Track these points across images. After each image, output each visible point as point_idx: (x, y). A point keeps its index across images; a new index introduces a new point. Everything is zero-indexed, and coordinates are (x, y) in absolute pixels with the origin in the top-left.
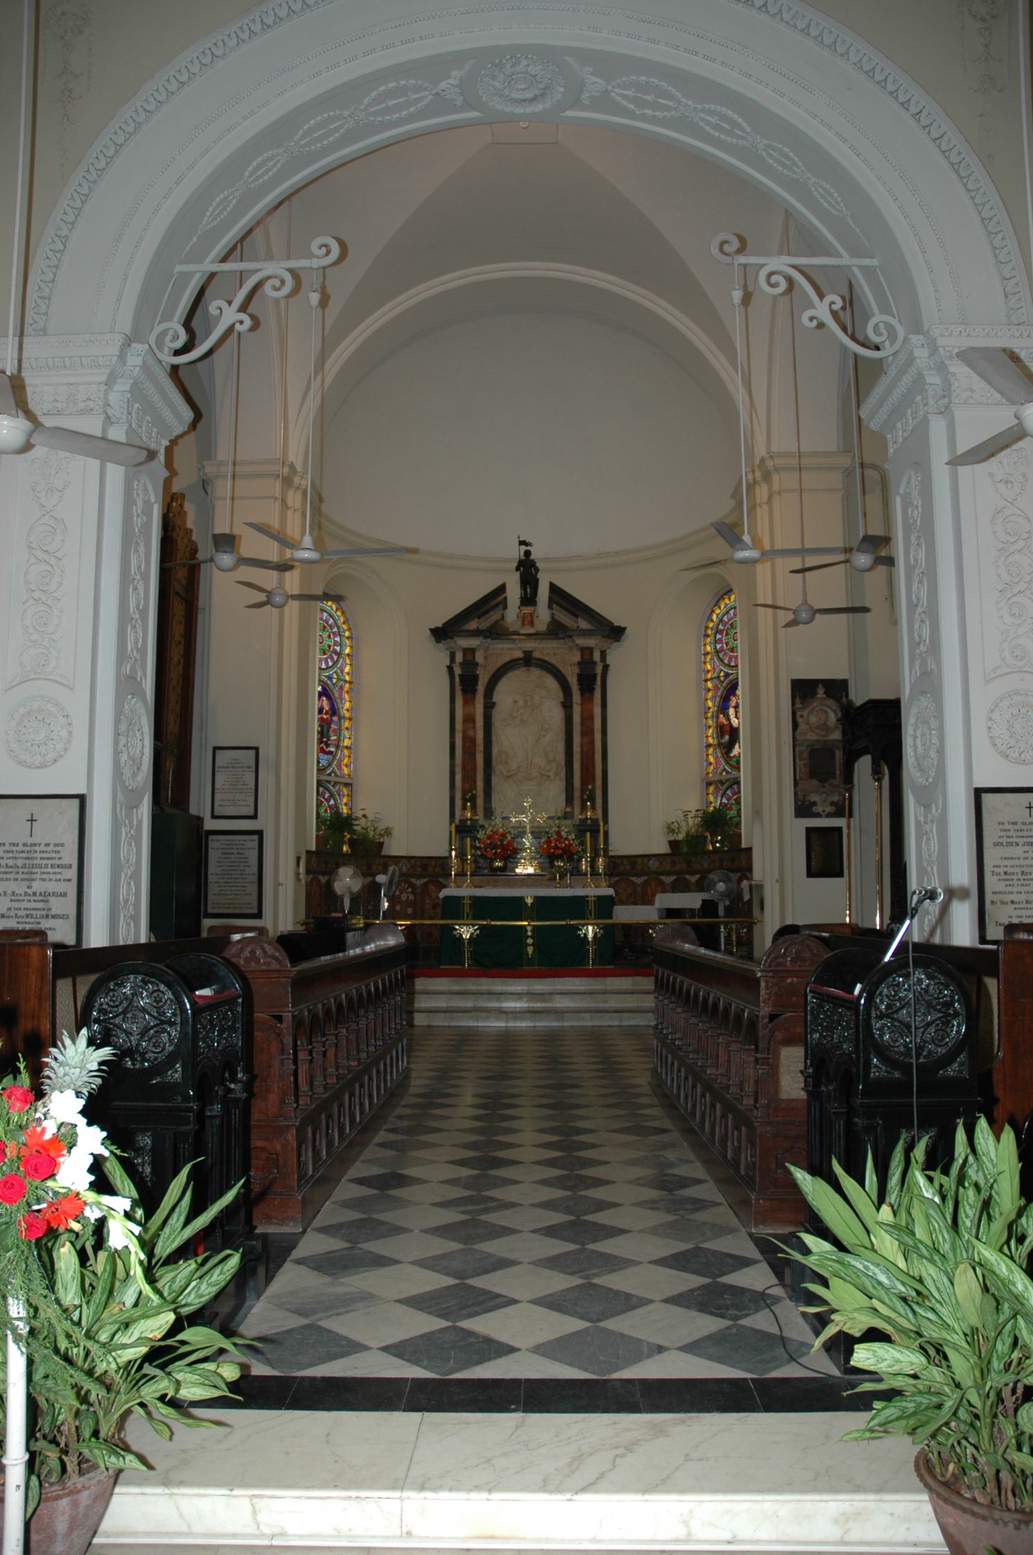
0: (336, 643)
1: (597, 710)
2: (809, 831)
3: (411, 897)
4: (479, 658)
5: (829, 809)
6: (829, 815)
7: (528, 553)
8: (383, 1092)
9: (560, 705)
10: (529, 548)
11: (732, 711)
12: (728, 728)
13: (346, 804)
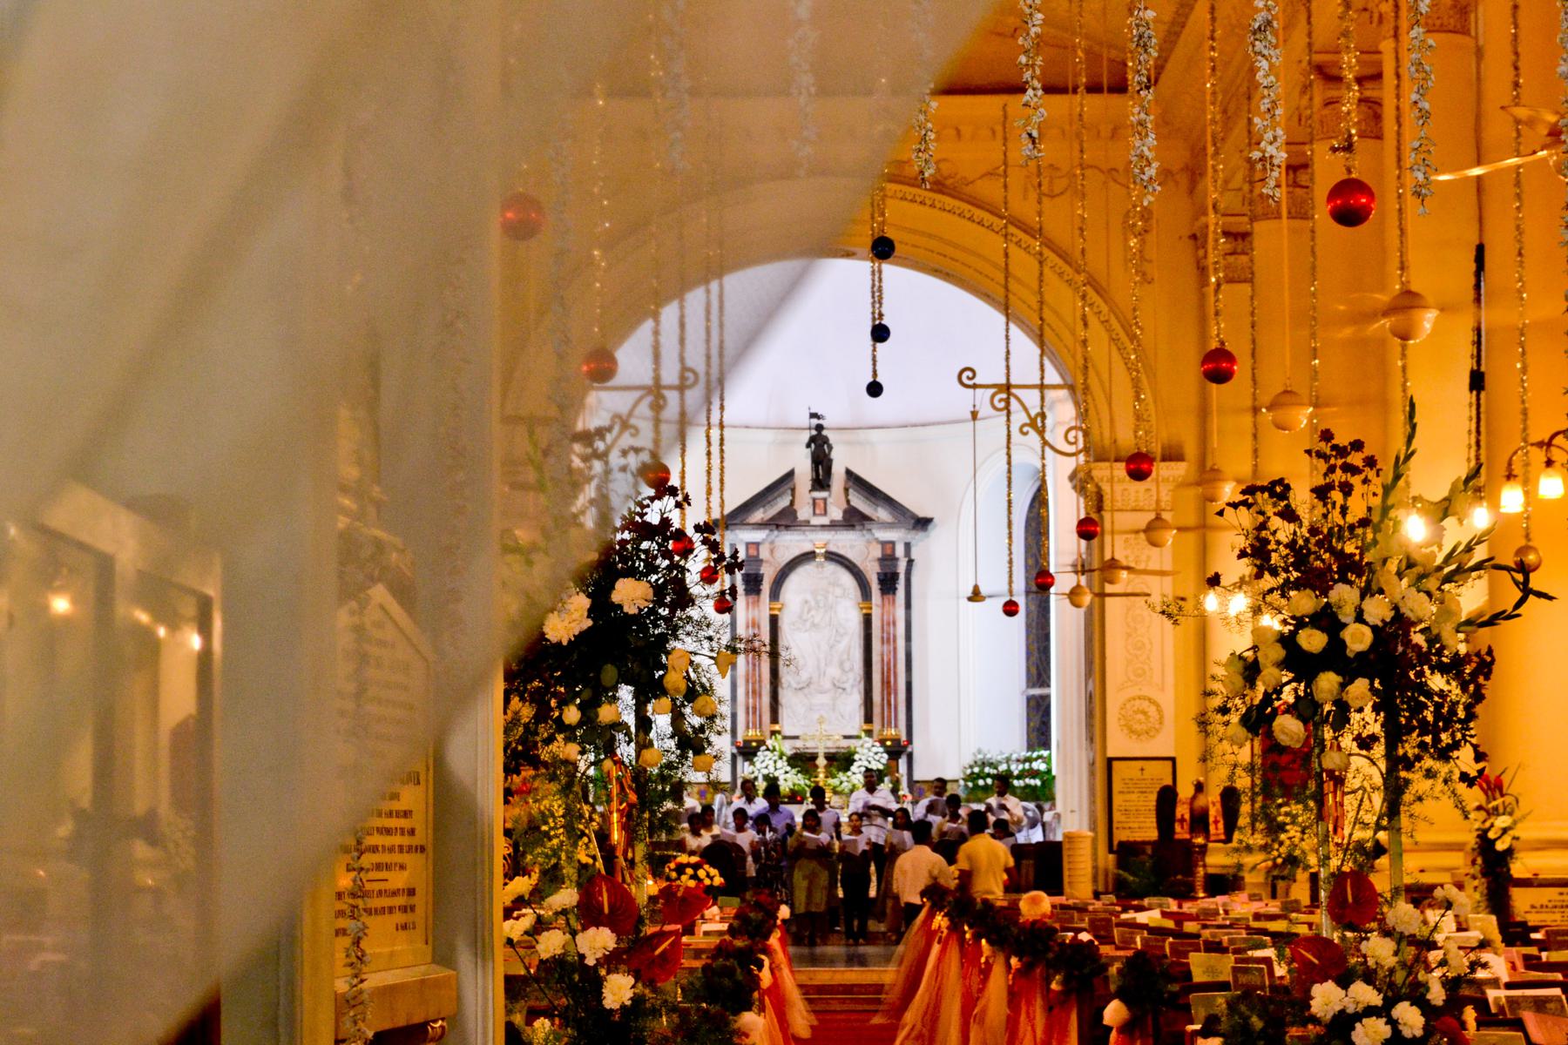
1: (900, 613)
4: (764, 553)
8: (1560, 938)
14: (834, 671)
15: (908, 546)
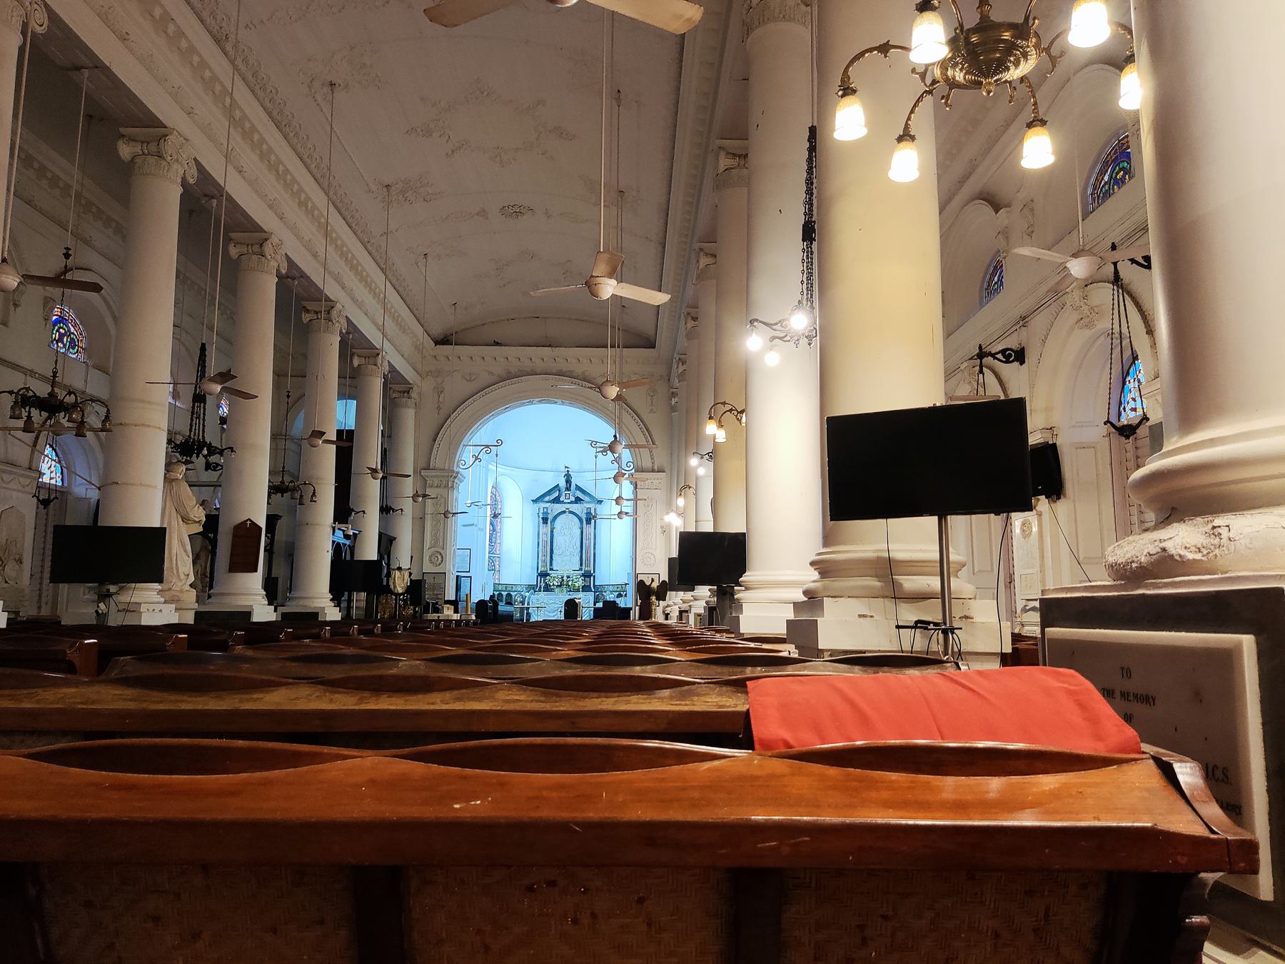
14: (571, 549)
15: (595, 509)
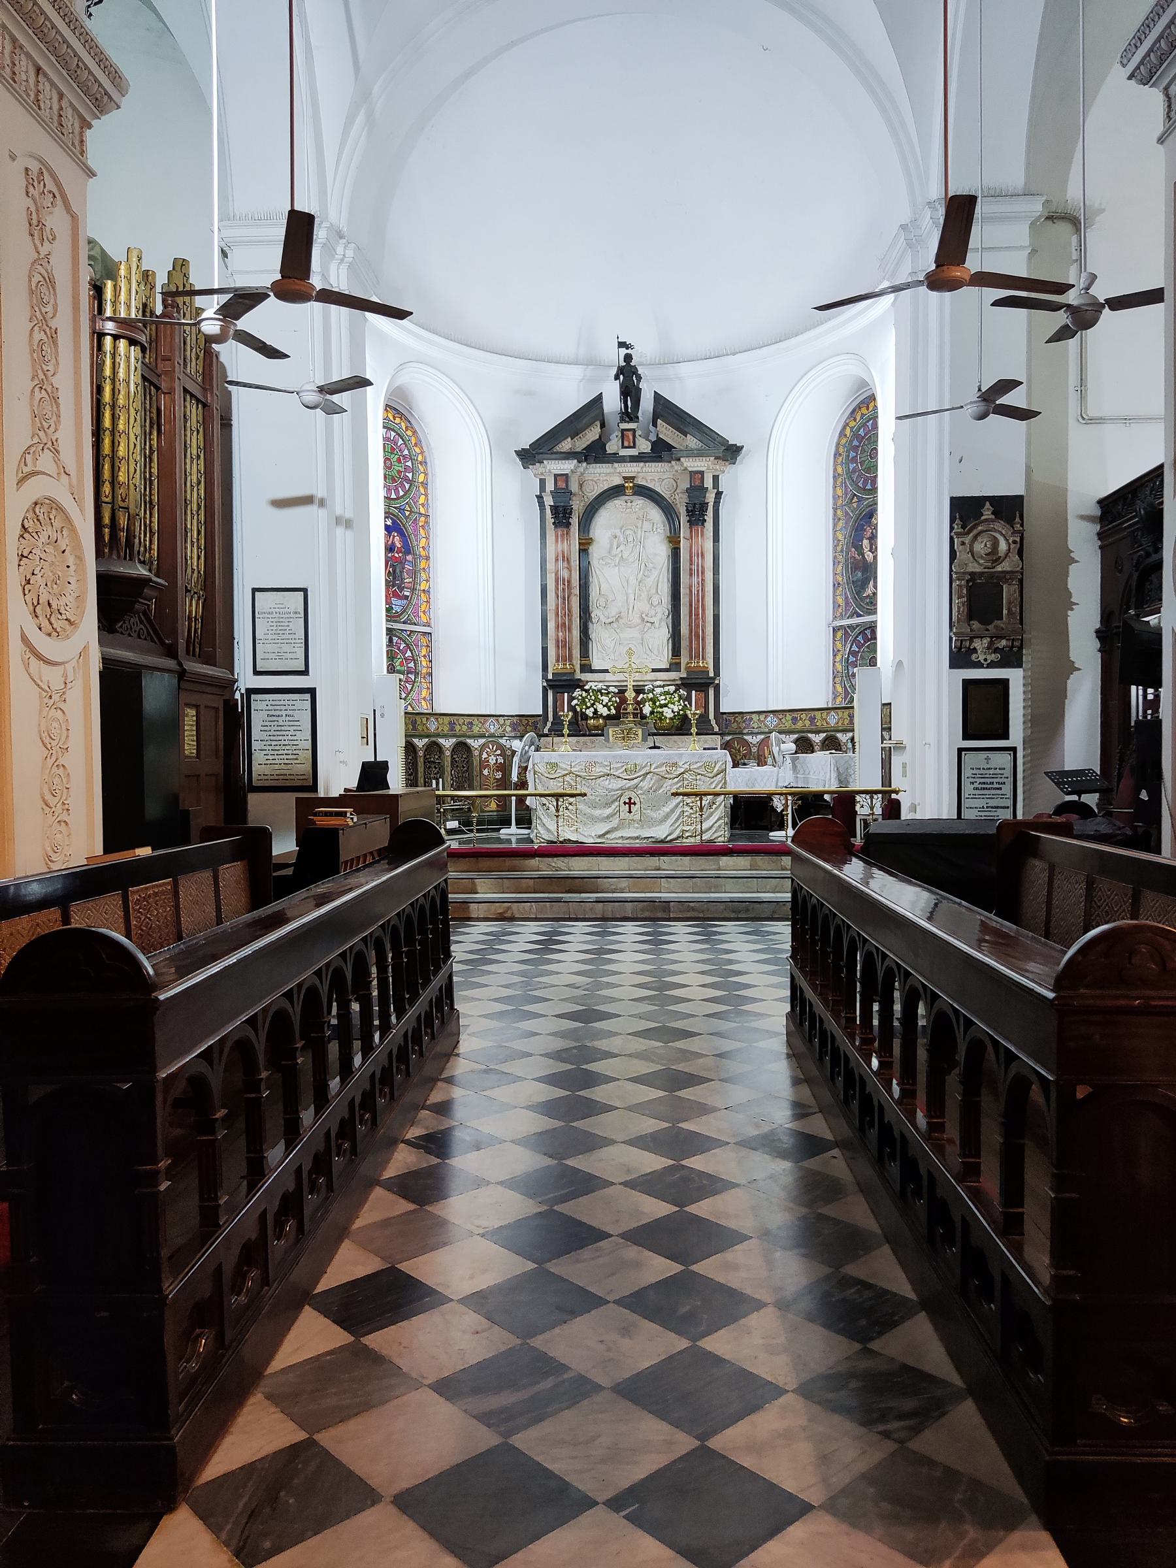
0: (407, 469)
2: (967, 684)
3: (501, 760)
5: (993, 657)
6: (992, 665)
7: (628, 358)
9: (666, 541)
10: (629, 351)
11: (866, 542)
12: (861, 565)
13: (424, 656)
